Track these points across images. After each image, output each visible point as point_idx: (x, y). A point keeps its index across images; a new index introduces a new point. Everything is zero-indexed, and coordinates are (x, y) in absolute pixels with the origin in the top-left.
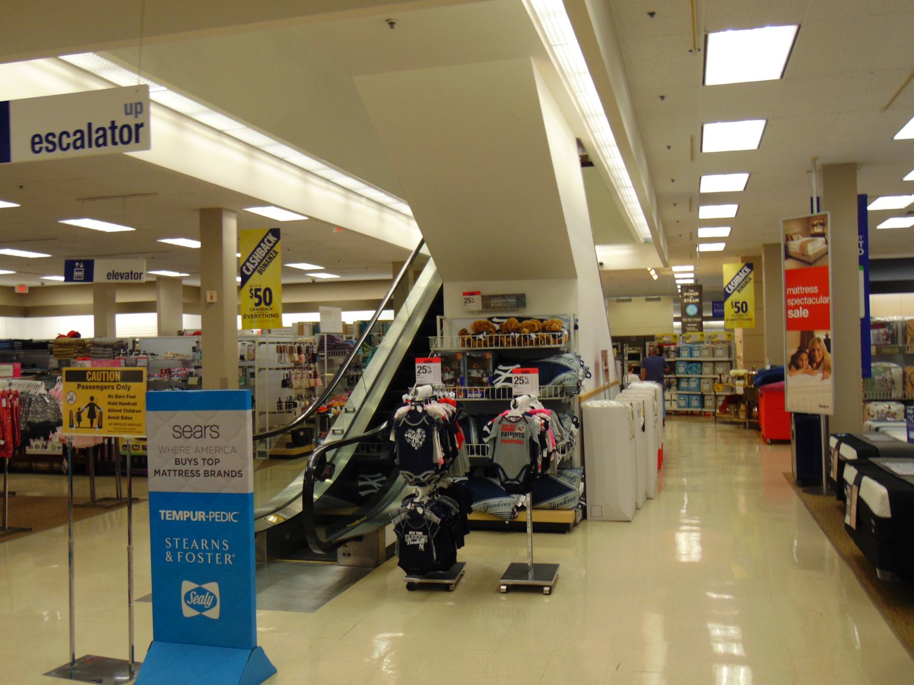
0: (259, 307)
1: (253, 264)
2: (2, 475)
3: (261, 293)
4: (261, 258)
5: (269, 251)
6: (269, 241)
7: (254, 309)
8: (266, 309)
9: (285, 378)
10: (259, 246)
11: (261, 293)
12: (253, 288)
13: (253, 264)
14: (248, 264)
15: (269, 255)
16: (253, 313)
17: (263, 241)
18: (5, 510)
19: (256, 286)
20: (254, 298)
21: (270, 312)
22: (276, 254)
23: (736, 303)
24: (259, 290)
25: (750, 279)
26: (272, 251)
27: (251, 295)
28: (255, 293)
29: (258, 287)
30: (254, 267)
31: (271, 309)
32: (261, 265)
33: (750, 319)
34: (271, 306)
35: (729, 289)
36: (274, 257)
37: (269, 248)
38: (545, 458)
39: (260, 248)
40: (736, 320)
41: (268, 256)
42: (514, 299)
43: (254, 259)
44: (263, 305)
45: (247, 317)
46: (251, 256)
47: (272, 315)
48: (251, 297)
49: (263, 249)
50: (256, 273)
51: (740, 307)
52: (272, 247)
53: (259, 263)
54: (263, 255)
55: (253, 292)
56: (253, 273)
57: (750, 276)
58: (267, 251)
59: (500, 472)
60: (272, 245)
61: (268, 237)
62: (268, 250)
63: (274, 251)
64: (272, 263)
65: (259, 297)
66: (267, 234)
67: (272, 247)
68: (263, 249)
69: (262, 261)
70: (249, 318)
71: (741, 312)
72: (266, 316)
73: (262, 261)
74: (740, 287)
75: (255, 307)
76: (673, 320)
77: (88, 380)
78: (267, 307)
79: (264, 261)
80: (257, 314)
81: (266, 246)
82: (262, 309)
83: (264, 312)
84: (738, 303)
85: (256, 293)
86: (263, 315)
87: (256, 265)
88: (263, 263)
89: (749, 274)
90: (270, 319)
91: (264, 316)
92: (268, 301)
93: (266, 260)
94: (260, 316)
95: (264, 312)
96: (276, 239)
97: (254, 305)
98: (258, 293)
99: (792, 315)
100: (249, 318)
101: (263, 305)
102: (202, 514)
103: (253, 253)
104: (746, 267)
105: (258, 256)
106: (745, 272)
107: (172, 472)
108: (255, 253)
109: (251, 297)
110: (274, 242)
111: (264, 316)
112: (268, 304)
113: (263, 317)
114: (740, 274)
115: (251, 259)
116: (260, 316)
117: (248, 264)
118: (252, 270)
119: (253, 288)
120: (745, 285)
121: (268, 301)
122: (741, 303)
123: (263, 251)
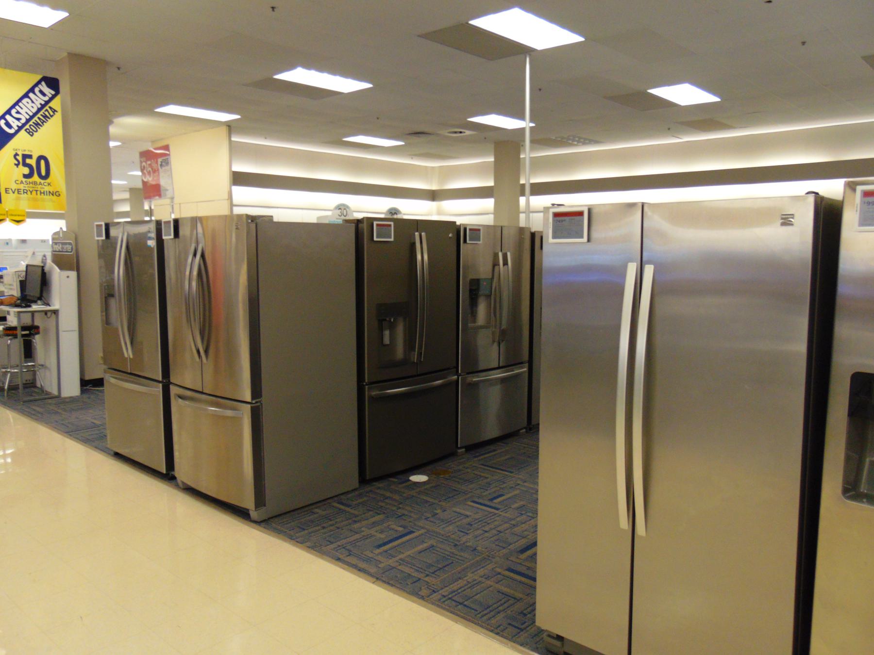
0: (30, 180)
1: (19, 119)
3: (32, 162)
4: (31, 114)
5: (43, 106)
7: (22, 182)
8: (40, 184)
10: (26, 95)
11: (32, 162)
12: (20, 153)
13: (19, 119)
14: (8, 117)
15: (43, 111)
16: (22, 187)
19: (25, 151)
20: (21, 166)
21: (47, 189)
22: (53, 112)
23: (25, 157)
25: (55, 111)
26: (47, 107)
27: (17, 163)
29: (26, 153)
30: (20, 125)
31: (49, 184)
32: (31, 123)
33: (56, 194)
34: (48, 181)
35: (8, 125)
36: (52, 116)
37: (43, 103)
38: (132, 359)
39: (25, 100)
40: (25, 192)
41: (41, 113)
42: (136, 170)
43: (18, 112)
45: (10, 192)
46: (13, 107)
47: (50, 192)
48: (17, 165)
49: (33, 102)
50: (23, 132)
51: (34, 165)
52: (47, 103)
53: (28, 121)
54: (34, 110)
55: (20, 158)
56: (17, 132)
57: (53, 104)
58: (39, 106)
59: (201, 326)
60: (46, 99)
61: (40, 86)
62: (41, 104)
63: (50, 108)
64: (48, 123)
65: (30, 166)
66: (39, 83)
67: (47, 103)
68: (33, 102)
69: (32, 117)
70: (14, 193)
71: (36, 177)
72: (41, 193)
73: (32, 117)
74: (33, 124)
75: (24, 180)
77: (12, 131)
78: (42, 181)
79: (36, 118)
80: (27, 188)
82: (35, 183)
83: (39, 187)
84: (30, 157)
85: (24, 161)
86: (36, 191)
87: (23, 121)
88: (33, 120)
89: (51, 99)
91: (39, 192)
92: (43, 173)
93: (39, 118)
94: (31, 192)
95: (39, 187)
96: (53, 92)
97: (22, 176)
98: (28, 161)
100: (14, 193)
103: (17, 103)
104: (43, 83)
105: (25, 109)
106: (41, 92)
108: (20, 104)
109: (17, 165)
110: (50, 96)
111: (39, 192)
113: (37, 194)
114: (31, 95)
115: (13, 112)
116: (31, 192)
117: (8, 117)
118: (16, 128)
119: (20, 153)
120: (43, 122)
121: (43, 173)
123: (33, 105)
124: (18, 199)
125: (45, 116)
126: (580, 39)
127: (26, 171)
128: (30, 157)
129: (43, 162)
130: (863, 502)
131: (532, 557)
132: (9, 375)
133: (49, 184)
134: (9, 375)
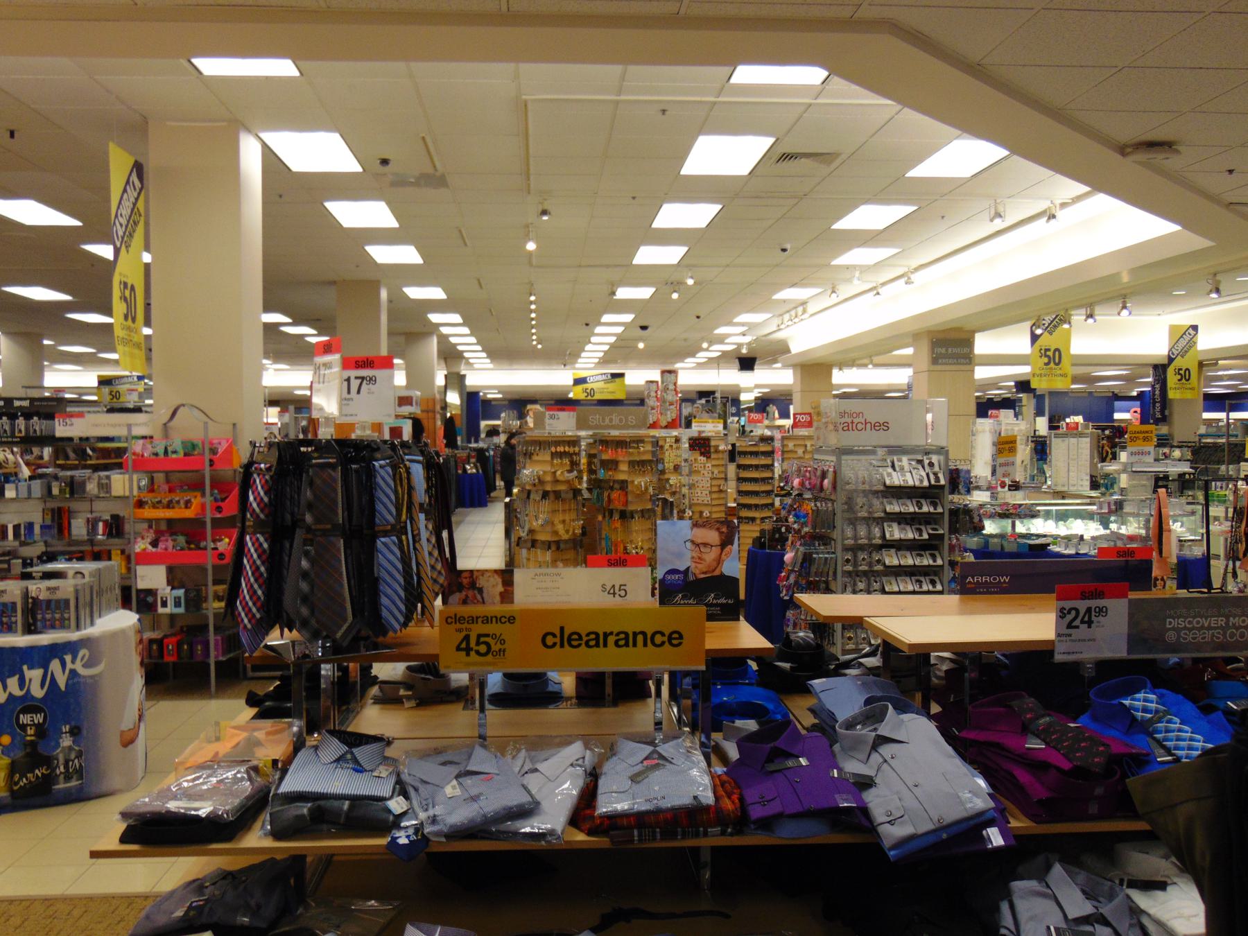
2: (1242, 503)
3: (1182, 372)
6: (1190, 334)
9: (421, 458)
10: (1182, 337)
11: (1182, 372)
16: (1043, 372)
17: (1185, 333)
18: (270, 671)
24: (1181, 369)
28: (1045, 352)
34: (1060, 366)
44: (1184, 381)
48: (1041, 357)
53: (1049, 324)
55: (1043, 352)
69: (1052, 322)
73: (1052, 322)
76: (154, 391)
77: (1173, 357)
81: (1187, 338)
82: (1051, 369)
84: (1049, 350)
90: (1059, 378)
92: (1057, 361)
98: (1048, 353)
99: (1183, 624)
101: (1184, 381)
102: (1222, 620)
107: (611, 639)
109: (1041, 357)
112: (1188, 380)
119: (1043, 348)
121: (1057, 361)
122: (1052, 351)
124: (1040, 381)
125: (1190, 347)
126: (912, 174)
127: (1046, 360)
128: (1049, 350)
129: (1057, 353)
130: (500, 389)
131: (698, 545)
132: (101, 524)
133: (1060, 369)
134: (101, 524)
